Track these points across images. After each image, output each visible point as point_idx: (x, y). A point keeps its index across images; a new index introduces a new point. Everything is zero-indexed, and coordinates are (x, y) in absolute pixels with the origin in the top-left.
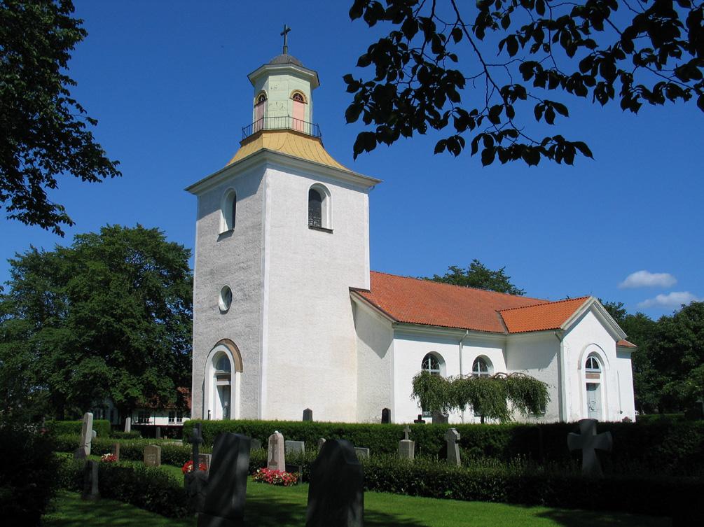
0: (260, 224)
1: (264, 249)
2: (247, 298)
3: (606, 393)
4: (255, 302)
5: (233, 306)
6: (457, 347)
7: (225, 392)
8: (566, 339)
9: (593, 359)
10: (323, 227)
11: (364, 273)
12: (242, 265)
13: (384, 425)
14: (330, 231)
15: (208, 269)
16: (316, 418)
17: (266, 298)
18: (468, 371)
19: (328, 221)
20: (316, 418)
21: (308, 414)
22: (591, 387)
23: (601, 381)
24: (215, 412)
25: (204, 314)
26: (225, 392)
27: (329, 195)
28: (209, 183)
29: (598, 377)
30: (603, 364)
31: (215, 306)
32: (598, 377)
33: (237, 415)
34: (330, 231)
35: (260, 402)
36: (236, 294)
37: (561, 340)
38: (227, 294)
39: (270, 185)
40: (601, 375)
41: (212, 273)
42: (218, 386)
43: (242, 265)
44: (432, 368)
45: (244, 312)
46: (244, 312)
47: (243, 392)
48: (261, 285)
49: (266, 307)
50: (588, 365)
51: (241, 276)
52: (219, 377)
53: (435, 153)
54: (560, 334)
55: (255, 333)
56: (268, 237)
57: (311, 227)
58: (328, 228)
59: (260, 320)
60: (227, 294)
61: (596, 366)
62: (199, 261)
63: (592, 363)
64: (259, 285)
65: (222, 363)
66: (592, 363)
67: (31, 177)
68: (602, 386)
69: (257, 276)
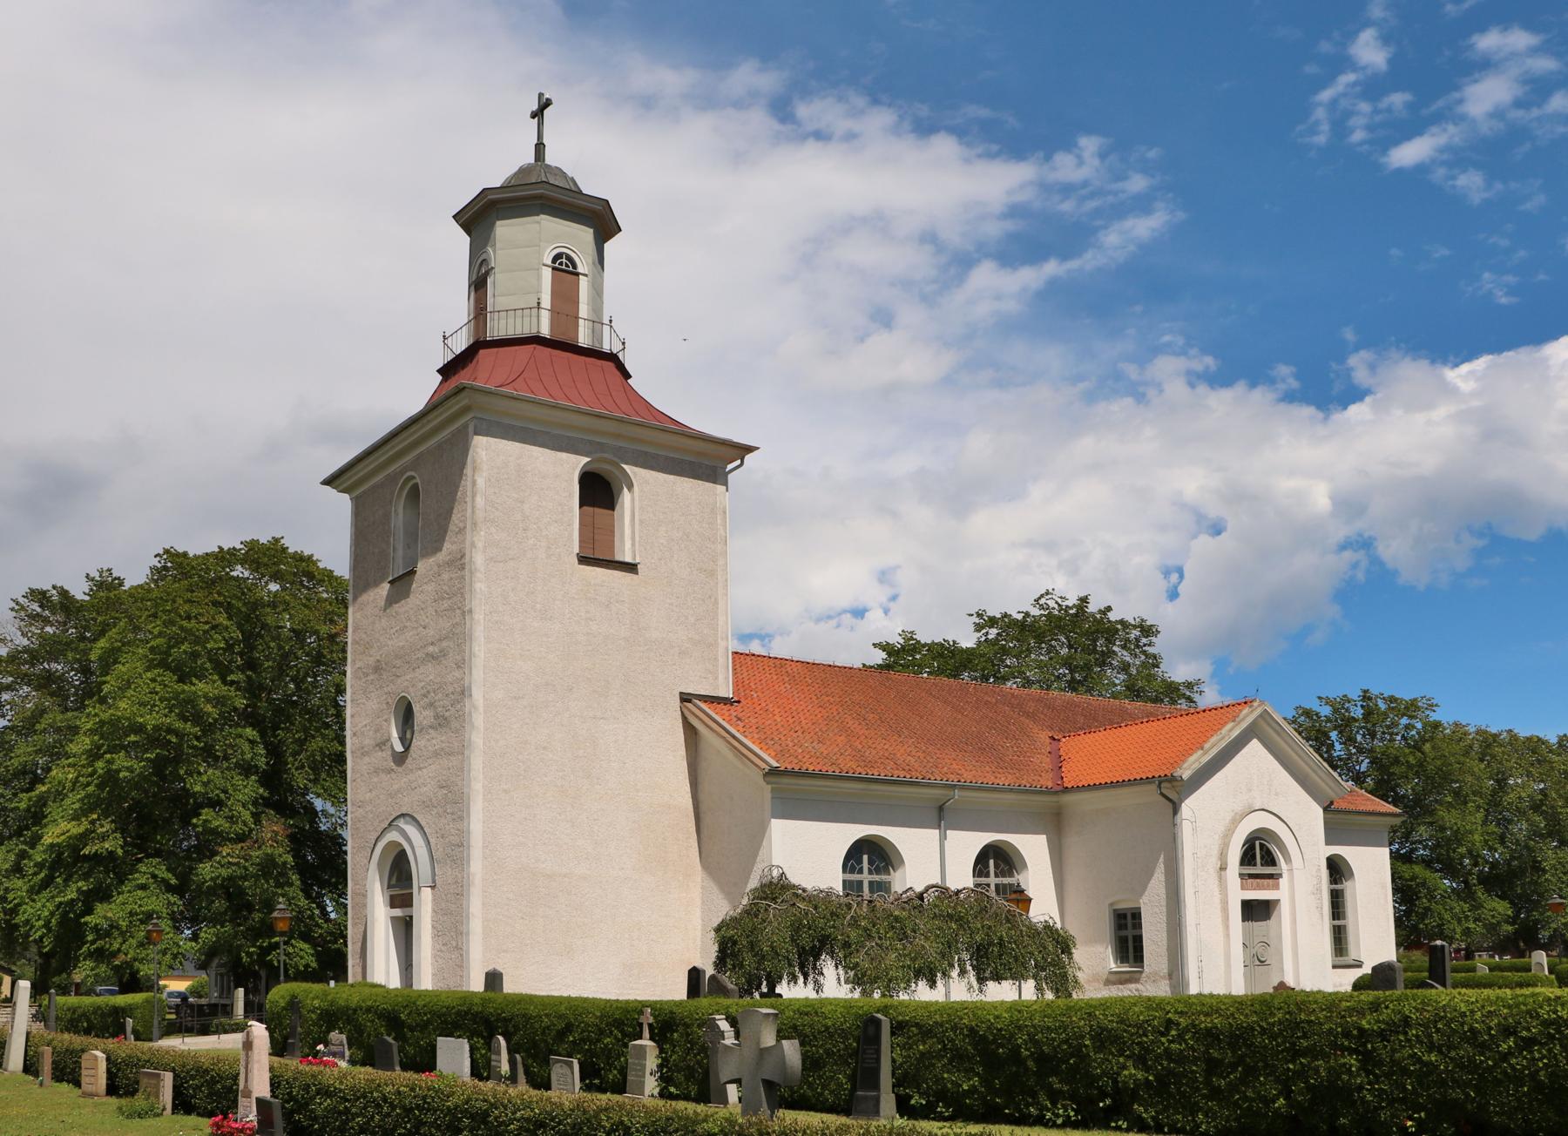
0: (463, 556)
1: (470, 611)
2: (442, 722)
3: (1294, 921)
4: (457, 731)
5: (418, 742)
6: (934, 834)
7: (405, 929)
8: (1189, 807)
9: (1262, 846)
10: (618, 558)
11: (716, 659)
12: (431, 649)
13: (490, 995)
14: (631, 568)
15: (371, 661)
16: (509, 987)
17: (479, 720)
18: (961, 877)
19: (628, 544)
20: (509, 987)
21: (493, 979)
22: (1256, 911)
23: (1280, 893)
24: (383, 970)
25: (367, 759)
26: (405, 929)
27: (630, 487)
28: (382, 457)
29: (1277, 887)
30: (1288, 859)
31: (384, 743)
32: (1277, 887)
33: (425, 980)
34: (631, 568)
35: (468, 952)
36: (422, 716)
37: (1176, 809)
38: (406, 715)
39: (485, 467)
40: (1283, 882)
41: (377, 669)
42: (394, 919)
43: (431, 649)
44: (870, 872)
45: (436, 754)
46: (436, 754)
47: (438, 933)
48: (464, 693)
49: (477, 738)
50: (1248, 858)
51: (429, 672)
52: (394, 902)
53: (329, 482)
54: (1171, 791)
55: (454, 802)
56: (480, 586)
57: (584, 560)
58: (628, 559)
59: (462, 770)
60: (406, 715)
61: (1270, 860)
62: (355, 642)
63: (1260, 854)
64: (463, 693)
65: (399, 872)
66: (1260, 854)
67: (1152, 154)
68: (1284, 909)
69: (457, 674)
